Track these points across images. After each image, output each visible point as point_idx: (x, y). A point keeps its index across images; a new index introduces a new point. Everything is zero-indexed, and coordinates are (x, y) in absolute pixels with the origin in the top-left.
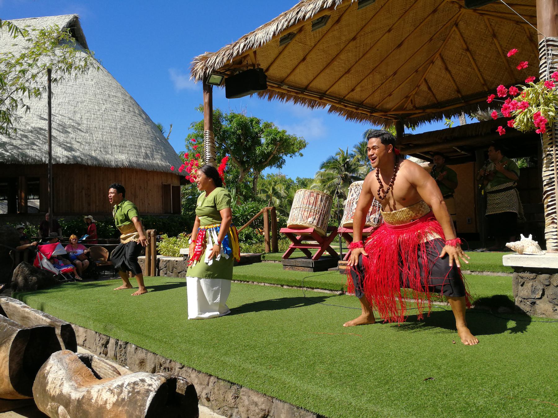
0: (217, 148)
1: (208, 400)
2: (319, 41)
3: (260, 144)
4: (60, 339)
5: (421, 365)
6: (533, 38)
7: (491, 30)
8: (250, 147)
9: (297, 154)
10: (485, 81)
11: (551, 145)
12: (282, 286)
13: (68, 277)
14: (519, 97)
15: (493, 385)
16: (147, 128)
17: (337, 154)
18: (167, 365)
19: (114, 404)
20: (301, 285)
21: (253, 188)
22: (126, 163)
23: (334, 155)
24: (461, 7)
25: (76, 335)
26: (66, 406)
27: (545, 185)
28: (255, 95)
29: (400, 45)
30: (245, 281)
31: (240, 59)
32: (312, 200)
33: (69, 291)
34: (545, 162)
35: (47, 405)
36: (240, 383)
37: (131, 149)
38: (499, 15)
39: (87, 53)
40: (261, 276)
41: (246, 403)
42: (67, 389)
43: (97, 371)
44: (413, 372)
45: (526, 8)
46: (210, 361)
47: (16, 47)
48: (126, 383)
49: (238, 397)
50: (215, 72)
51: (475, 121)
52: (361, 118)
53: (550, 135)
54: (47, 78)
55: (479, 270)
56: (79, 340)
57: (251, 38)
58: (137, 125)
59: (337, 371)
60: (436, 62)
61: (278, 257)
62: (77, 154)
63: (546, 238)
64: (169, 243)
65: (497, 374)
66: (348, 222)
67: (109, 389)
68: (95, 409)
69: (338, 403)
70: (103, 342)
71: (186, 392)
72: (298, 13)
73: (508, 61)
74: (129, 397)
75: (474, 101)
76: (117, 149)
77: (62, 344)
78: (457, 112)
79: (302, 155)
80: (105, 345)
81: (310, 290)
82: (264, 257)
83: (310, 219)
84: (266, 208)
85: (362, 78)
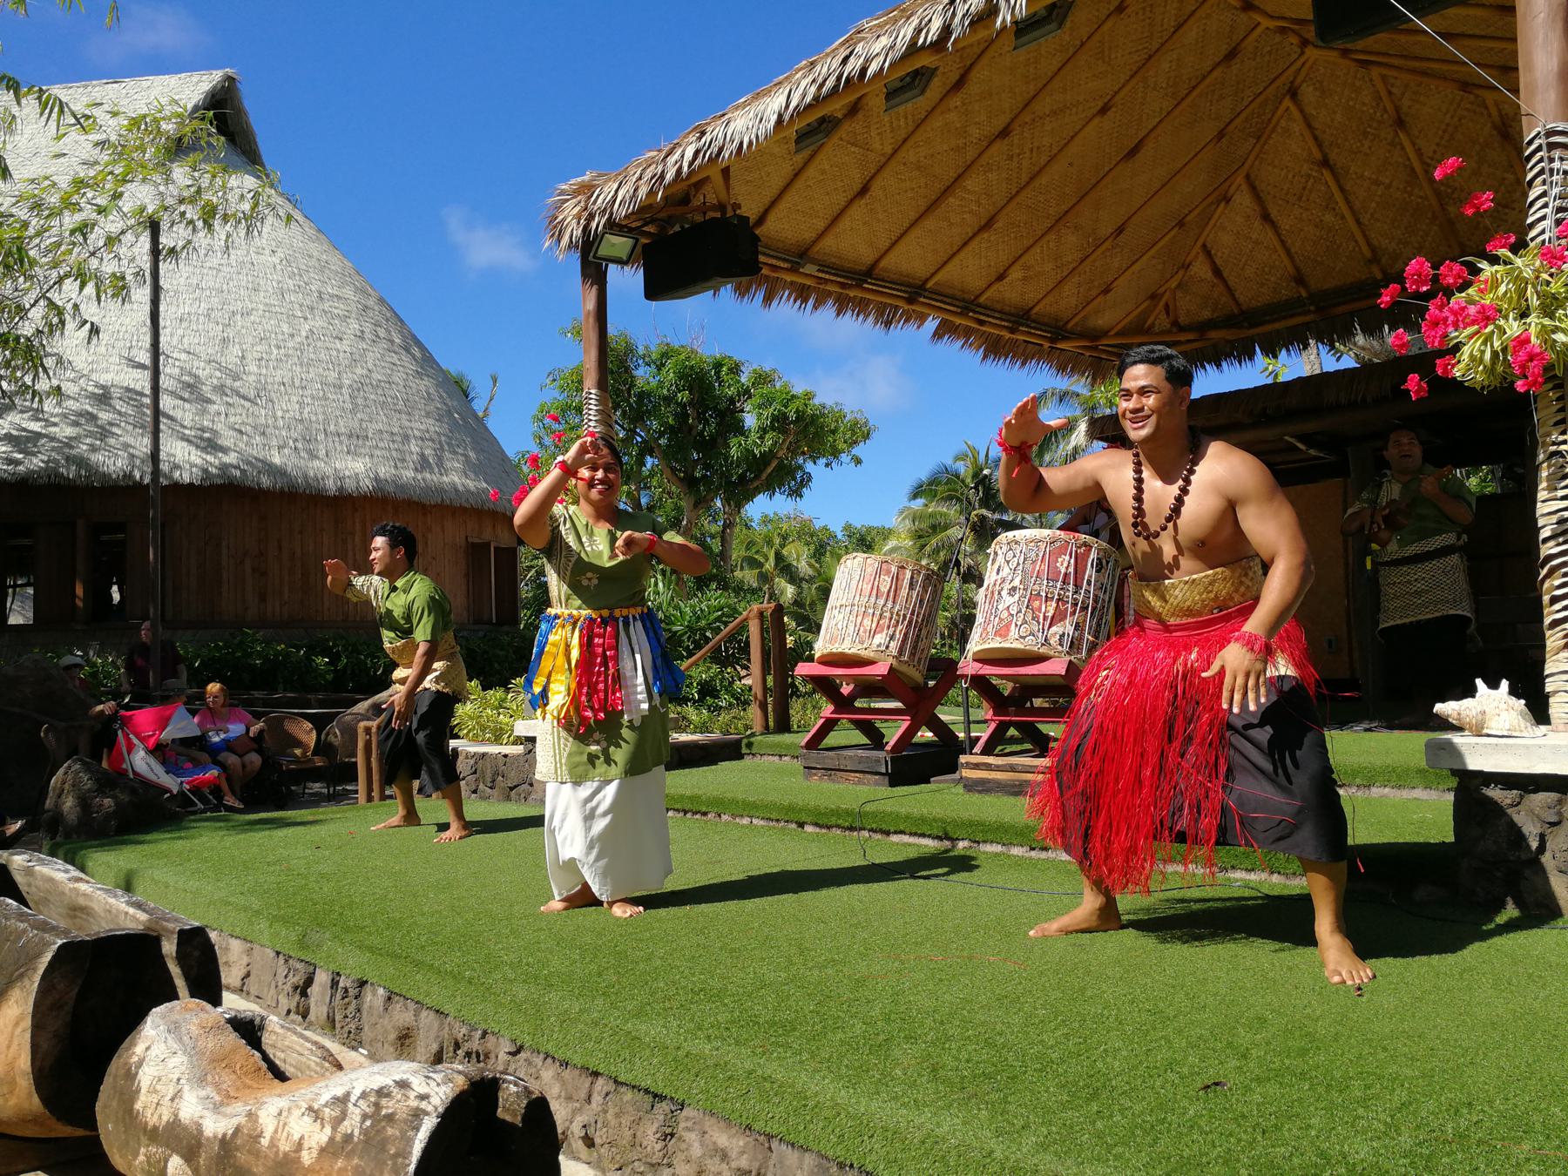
0: (623, 440)
1: (589, 1142)
2: (905, 140)
3: (740, 430)
4: (175, 970)
5: (1191, 1045)
6: (1508, 129)
7: (1389, 106)
8: (713, 439)
9: (844, 457)
10: (1373, 250)
11: (1562, 427)
12: (801, 825)
13: (203, 799)
14: (1471, 291)
15: (1396, 1102)
16: (425, 384)
17: (957, 458)
18: (475, 1045)
19: (322, 1150)
20: (853, 823)
21: (722, 552)
22: (367, 484)
23: (949, 462)
24: (1305, 43)
25: (221, 961)
26: (190, 1156)
27: (1545, 540)
28: (727, 291)
29: (1133, 153)
30: (695, 813)
31: (684, 191)
32: (886, 583)
33: (204, 839)
34: (1544, 474)
35: (136, 1154)
36: (680, 1096)
37: (381, 445)
38: (1416, 64)
39: (258, 177)
40: (740, 797)
41: (696, 1151)
42: (192, 1108)
43: (278, 1058)
44: (1170, 1065)
45: (1491, 44)
46: (595, 1034)
47: (62, 160)
48: (357, 1093)
49: (672, 1135)
50: (613, 226)
51: (1348, 362)
52: (1024, 354)
53: (1558, 399)
54: (147, 246)
55: (1358, 781)
56: (230, 975)
57: (716, 132)
58: (398, 378)
59: (951, 1063)
60: (1237, 198)
61: (788, 747)
62: (231, 458)
63: (1548, 689)
64: (485, 704)
65: (1409, 1072)
66: (986, 646)
67: (310, 1109)
68: (270, 1163)
69: (953, 1153)
70: (298, 979)
71: (525, 1118)
72: (845, 60)
73: (1438, 194)
74: (365, 1132)
75: (1341, 309)
76: (341, 443)
77: (180, 983)
78: (1296, 339)
79: (858, 461)
80: (303, 989)
81: (878, 836)
82: (750, 745)
83: (880, 638)
84: (755, 607)
85: (1027, 243)
